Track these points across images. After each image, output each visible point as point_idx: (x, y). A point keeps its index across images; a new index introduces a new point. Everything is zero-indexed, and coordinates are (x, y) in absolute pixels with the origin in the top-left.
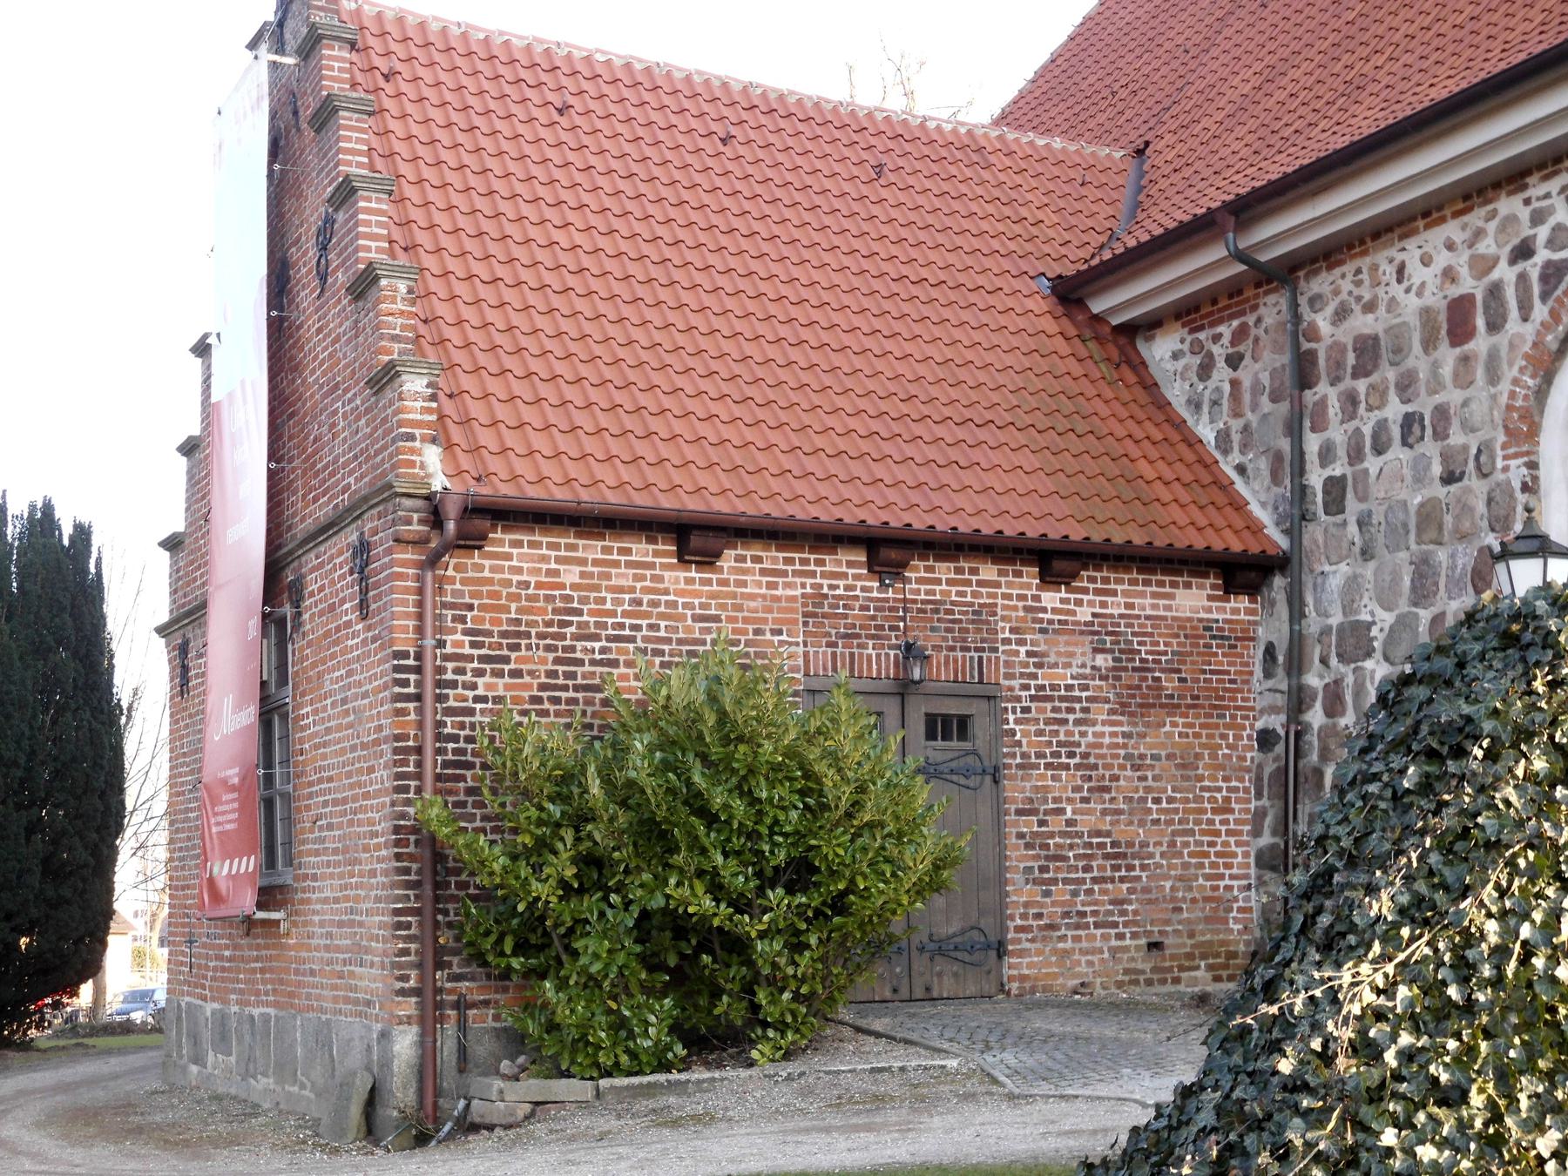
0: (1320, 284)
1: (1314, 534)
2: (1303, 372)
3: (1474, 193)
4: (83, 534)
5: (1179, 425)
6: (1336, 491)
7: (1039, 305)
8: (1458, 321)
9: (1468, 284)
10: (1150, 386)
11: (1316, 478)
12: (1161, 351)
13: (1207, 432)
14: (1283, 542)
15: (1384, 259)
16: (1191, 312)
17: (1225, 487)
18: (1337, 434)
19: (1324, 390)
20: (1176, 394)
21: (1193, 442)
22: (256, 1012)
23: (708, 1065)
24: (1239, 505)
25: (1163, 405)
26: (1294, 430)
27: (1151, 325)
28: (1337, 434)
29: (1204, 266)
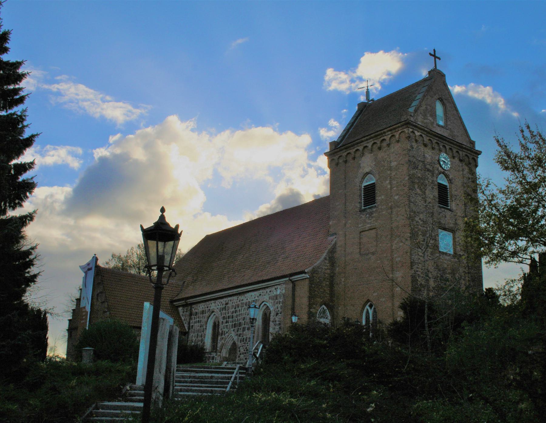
0: (193, 306)
1: (190, 331)
2: (191, 314)
3: (378, 132)
4: (33, 279)
5: (180, 317)
6: (192, 326)
7: (168, 303)
8: (203, 312)
9: (204, 309)
10: (178, 313)
11: (191, 325)
12: (180, 309)
13: (183, 318)
14: (187, 330)
15: (199, 305)
16: (183, 306)
17: (183, 325)
18: (193, 321)
19: (193, 317)
20: (181, 313)
21: (181, 319)
22: (234, 375)
23: (124, 103)
24: (184, 327)
25: (179, 315)
26: (190, 320)
27: (179, 306)
28: (193, 321)
29: (183, 302)
